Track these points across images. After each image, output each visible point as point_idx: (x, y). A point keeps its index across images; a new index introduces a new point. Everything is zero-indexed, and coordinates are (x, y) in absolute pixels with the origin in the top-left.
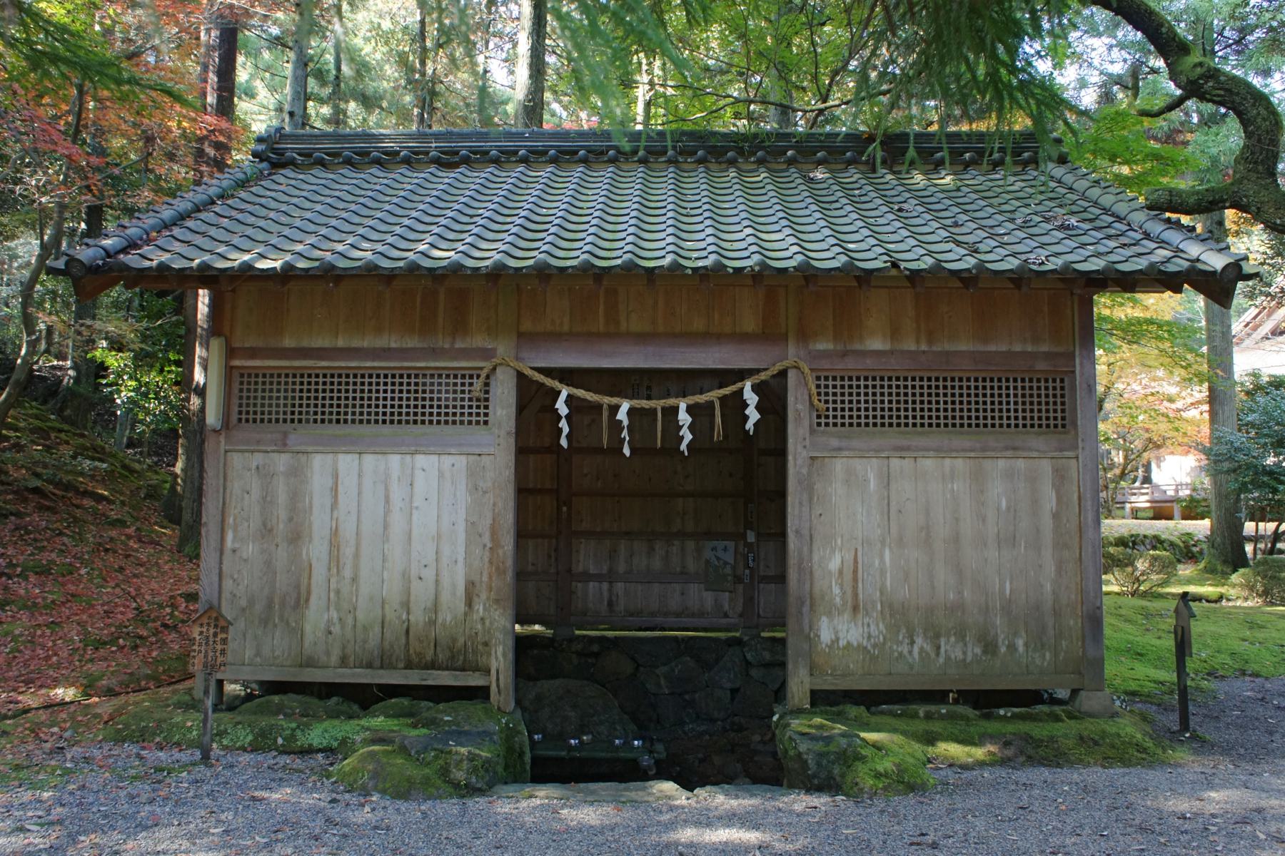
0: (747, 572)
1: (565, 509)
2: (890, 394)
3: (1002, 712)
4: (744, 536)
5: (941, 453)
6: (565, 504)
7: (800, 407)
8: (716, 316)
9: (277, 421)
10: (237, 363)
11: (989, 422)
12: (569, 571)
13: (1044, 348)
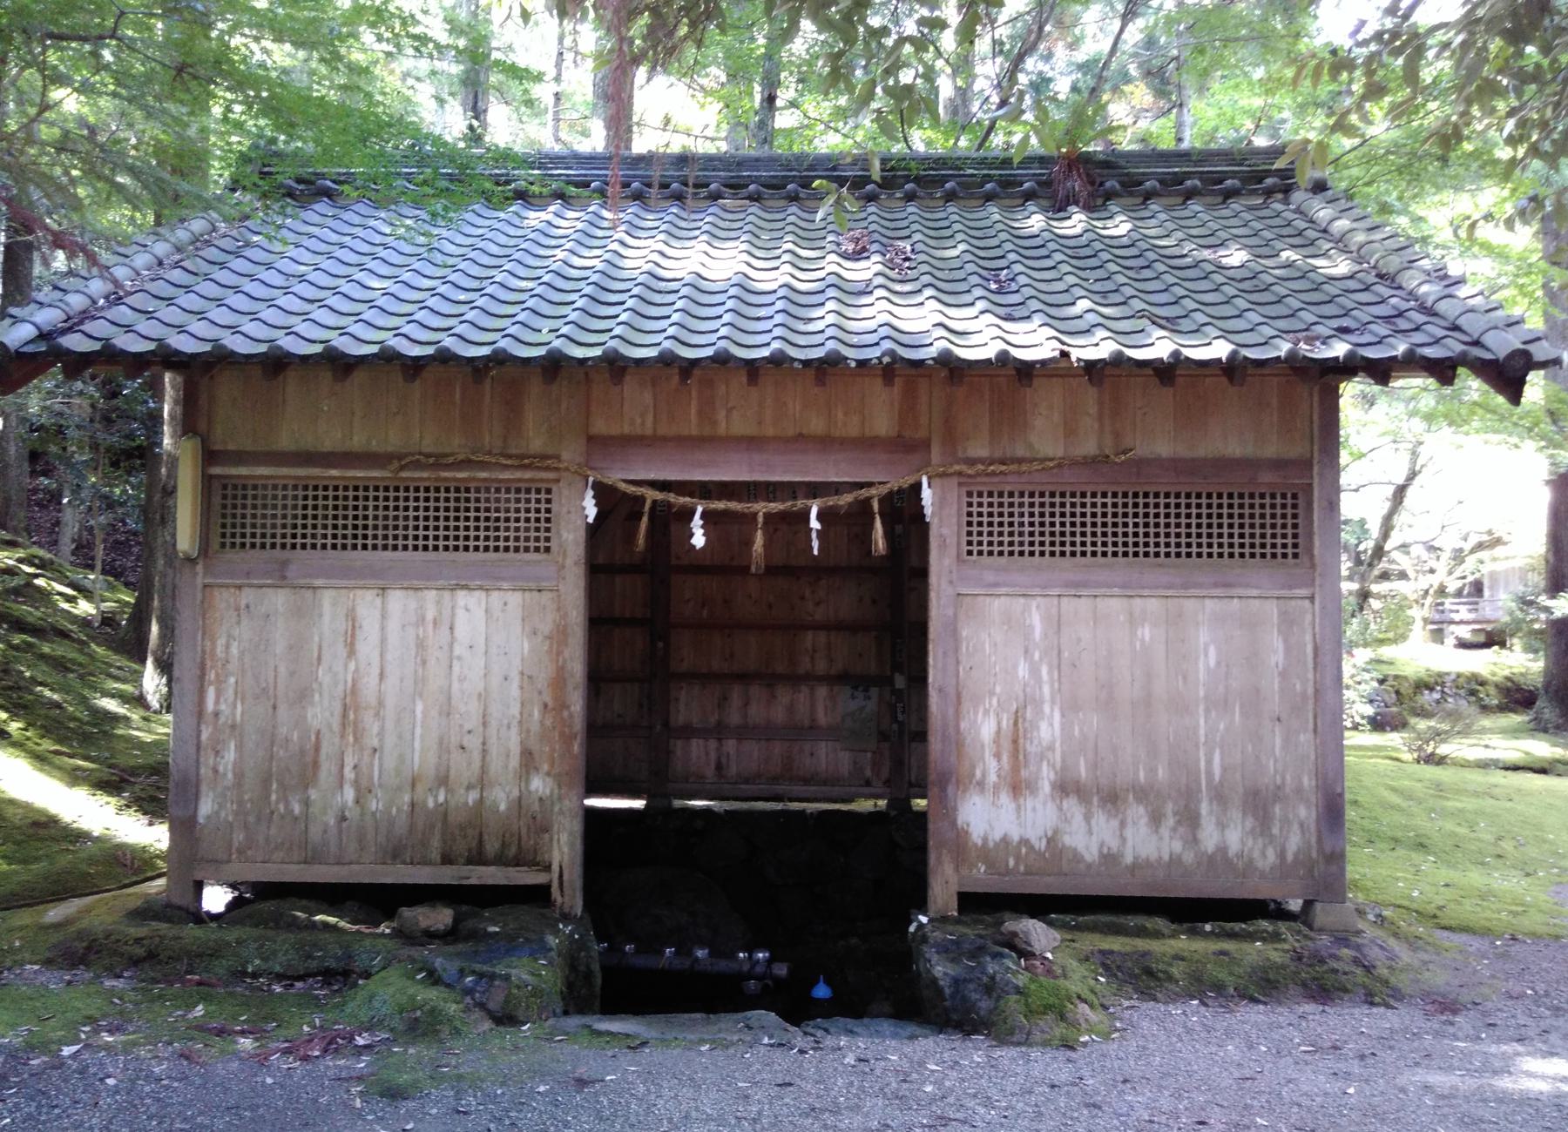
0: (895, 727)
2: (1063, 515)
3: (1208, 927)
4: (891, 681)
5: (1130, 590)
7: (945, 531)
8: (840, 415)
9: (273, 546)
10: (216, 470)
11: (1194, 550)
13: (1271, 451)
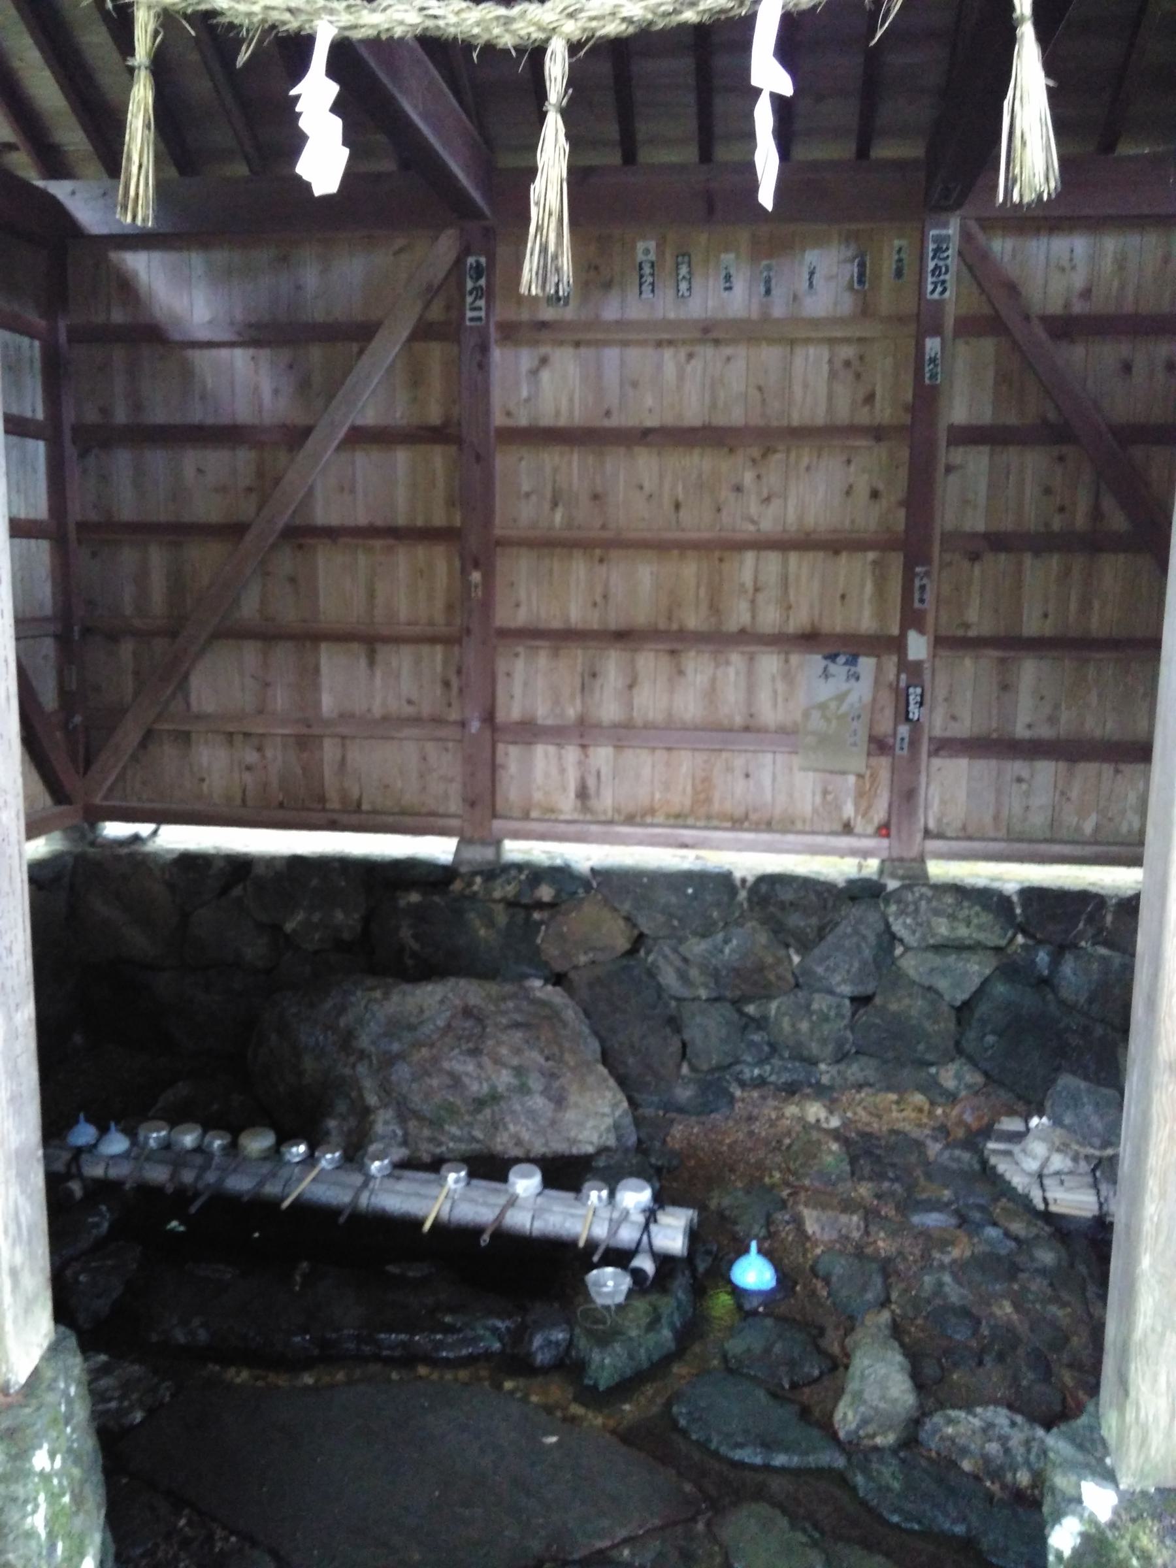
1: (476, 576)
4: (898, 645)
6: (476, 565)
12: (489, 718)
